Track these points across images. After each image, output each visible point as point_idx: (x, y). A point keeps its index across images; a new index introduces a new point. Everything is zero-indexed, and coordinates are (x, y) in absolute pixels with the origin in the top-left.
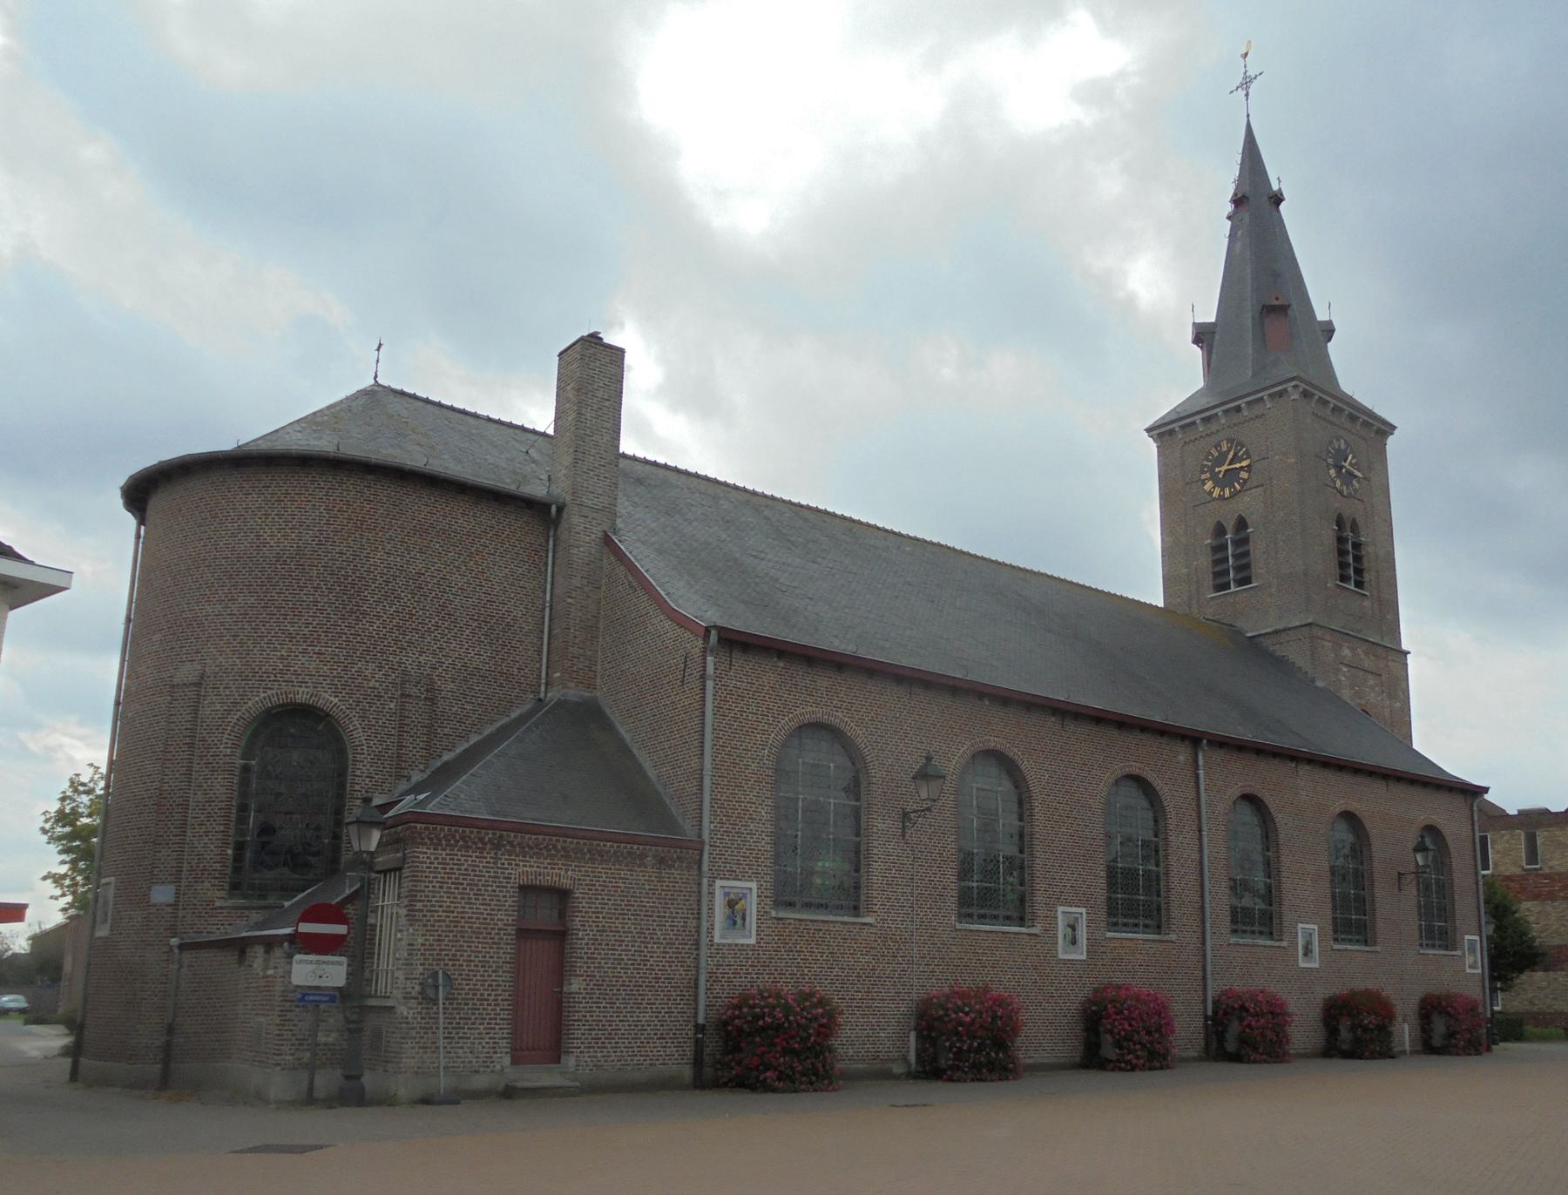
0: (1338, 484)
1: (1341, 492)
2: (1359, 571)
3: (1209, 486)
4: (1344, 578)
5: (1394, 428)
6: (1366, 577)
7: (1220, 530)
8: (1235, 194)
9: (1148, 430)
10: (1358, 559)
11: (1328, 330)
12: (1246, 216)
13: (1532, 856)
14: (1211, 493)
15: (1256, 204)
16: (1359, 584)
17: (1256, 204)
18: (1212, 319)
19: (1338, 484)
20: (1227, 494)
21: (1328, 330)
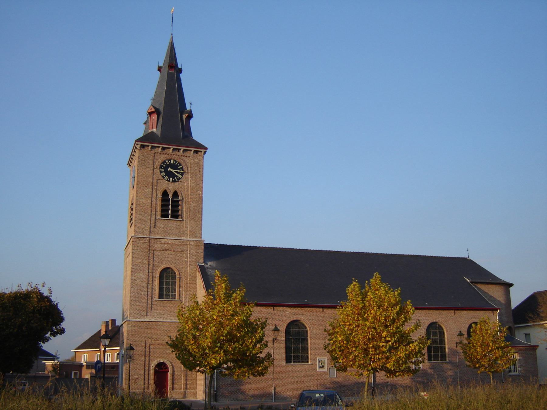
15: (172, 70)
17: (172, 70)
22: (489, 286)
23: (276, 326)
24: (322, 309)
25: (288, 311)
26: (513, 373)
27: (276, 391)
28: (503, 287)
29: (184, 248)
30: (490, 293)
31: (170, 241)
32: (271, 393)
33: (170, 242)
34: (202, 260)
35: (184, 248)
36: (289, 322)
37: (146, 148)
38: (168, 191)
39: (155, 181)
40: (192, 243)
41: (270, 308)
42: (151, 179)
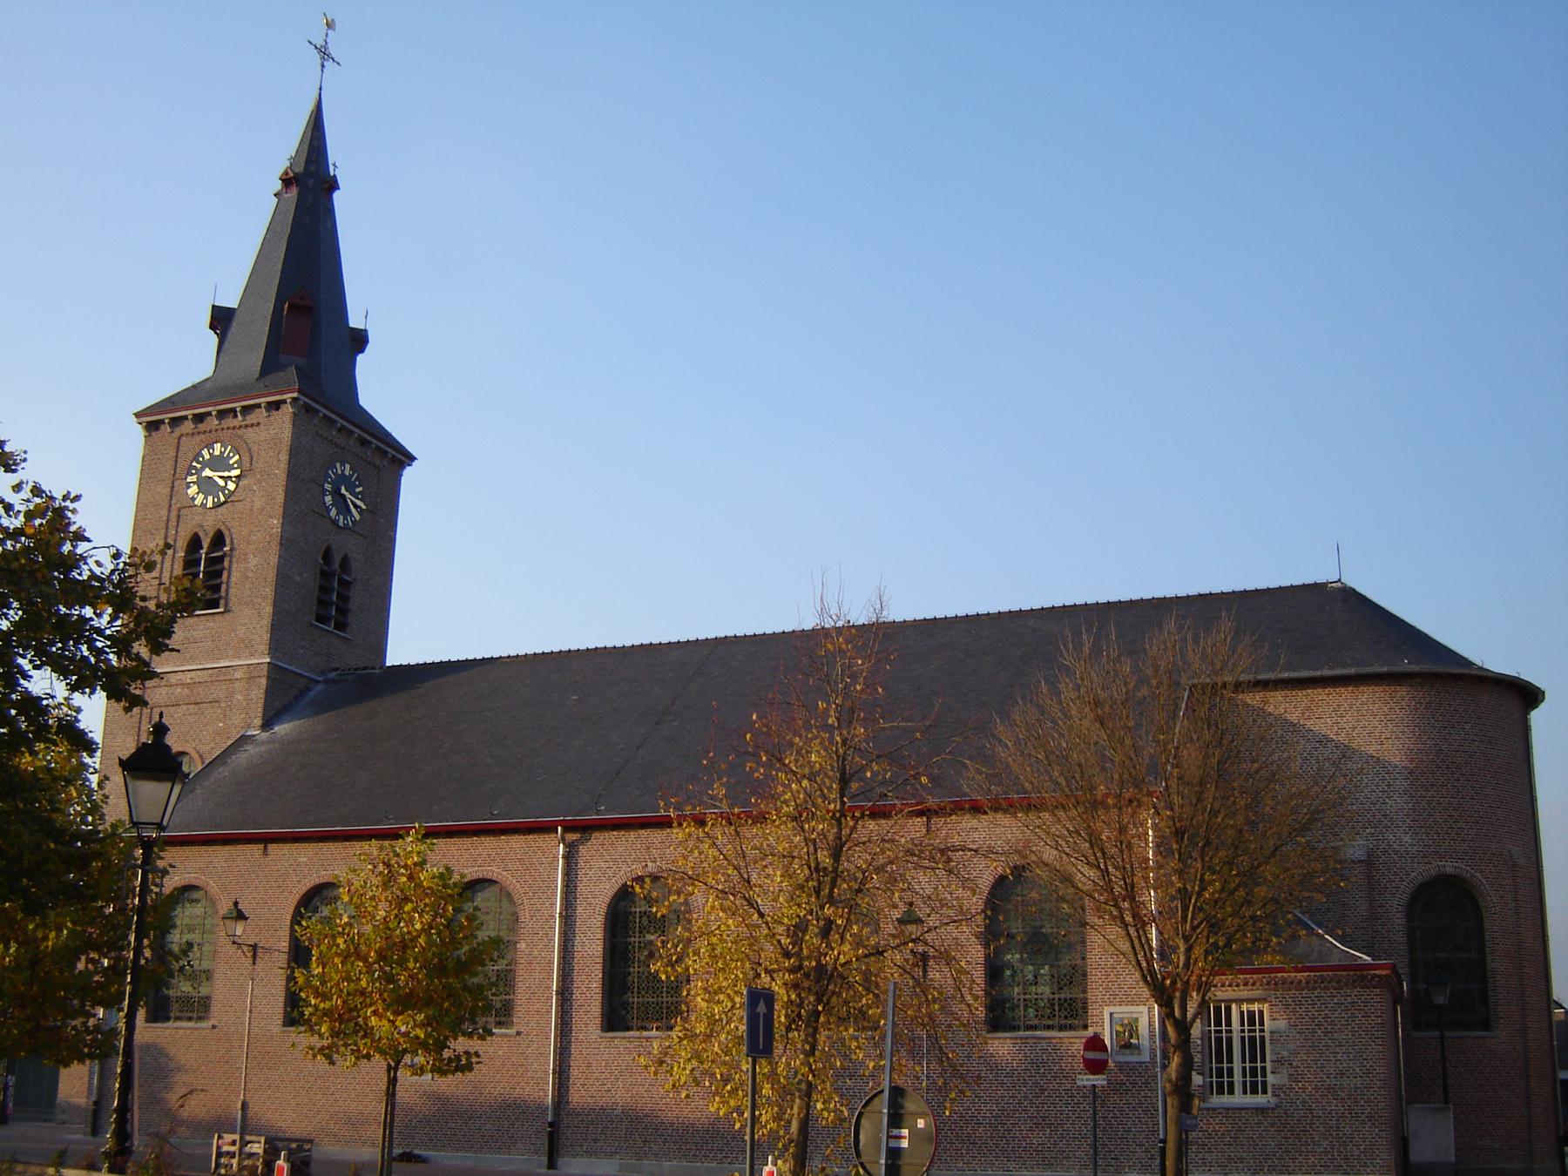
0: (333, 513)
1: (335, 523)
2: (343, 611)
3: (193, 490)
4: (321, 619)
5: (413, 459)
6: (351, 619)
7: (195, 543)
8: (286, 173)
9: (137, 415)
10: (344, 598)
11: (359, 340)
12: (294, 193)
13: (1442, 1038)
14: (193, 499)
15: (311, 184)
16: (341, 626)
17: (311, 184)
18: (235, 305)
19: (333, 513)
20: (205, 452)
21: (359, 340)
22: (1319, 694)
23: (236, 904)
24: (261, 846)
25: (303, 854)
26: (1239, 1099)
27: (250, 1113)
28: (1402, 691)
29: (220, 691)
30: (1323, 724)
31: (189, 675)
32: (235, 1119)
33: (188, 678)
34: (258, 722)
35: (220, 691)
36: (304, 889)
37: (283, 407)
38: (201, 535)
39: (174, 514)
40: (238, 675)
41: (256, 849)
42: (165, 512)
